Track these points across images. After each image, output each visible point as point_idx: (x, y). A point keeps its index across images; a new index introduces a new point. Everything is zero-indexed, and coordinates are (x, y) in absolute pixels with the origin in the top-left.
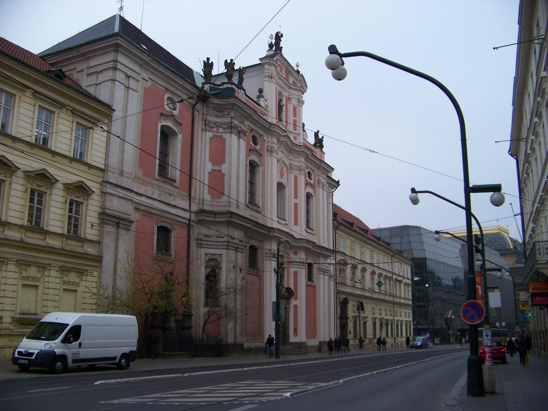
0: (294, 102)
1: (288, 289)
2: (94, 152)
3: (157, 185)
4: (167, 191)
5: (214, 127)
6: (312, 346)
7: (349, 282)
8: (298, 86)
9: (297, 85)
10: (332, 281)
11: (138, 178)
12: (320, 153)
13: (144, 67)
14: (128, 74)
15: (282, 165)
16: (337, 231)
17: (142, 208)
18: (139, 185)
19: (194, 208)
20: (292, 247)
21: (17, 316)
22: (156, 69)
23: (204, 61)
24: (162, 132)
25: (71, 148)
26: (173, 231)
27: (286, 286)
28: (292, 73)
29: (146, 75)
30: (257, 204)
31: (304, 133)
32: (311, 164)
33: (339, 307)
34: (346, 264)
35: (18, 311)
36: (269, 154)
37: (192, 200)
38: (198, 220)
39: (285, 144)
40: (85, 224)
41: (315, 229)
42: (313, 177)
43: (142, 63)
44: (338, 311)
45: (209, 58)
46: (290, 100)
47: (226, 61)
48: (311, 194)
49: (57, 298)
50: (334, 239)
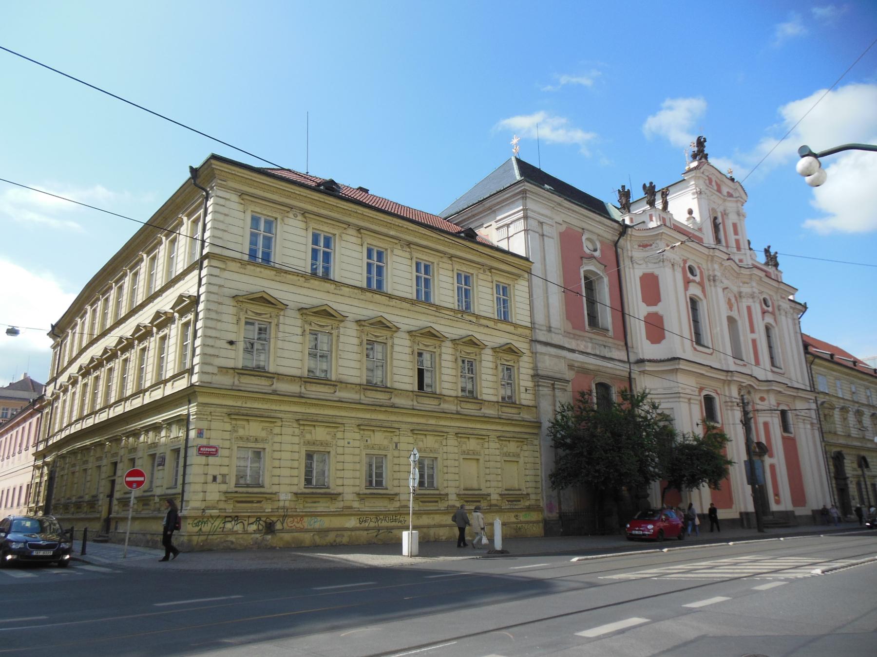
1: (759, 444)
2: (518, 311)
4: (601, 343)
6: (800, 516)
7: (840, 430)
10: (815, 431)
16: (812, 366)
18: (570, 340)
19: (633, 358)
21: (463, 492)
24: (586, 278)
25: (494, 310)
26: (613, 387)
27: (756, 441)
33: (831, 463)
34: (833, 408)
35: (462, 487)
36: (712, 283)
37: (629, 349)
40: (519, 389)
41: (783, 367)
42: (698, 272)
47: (644, 186)
49: (499, 471)
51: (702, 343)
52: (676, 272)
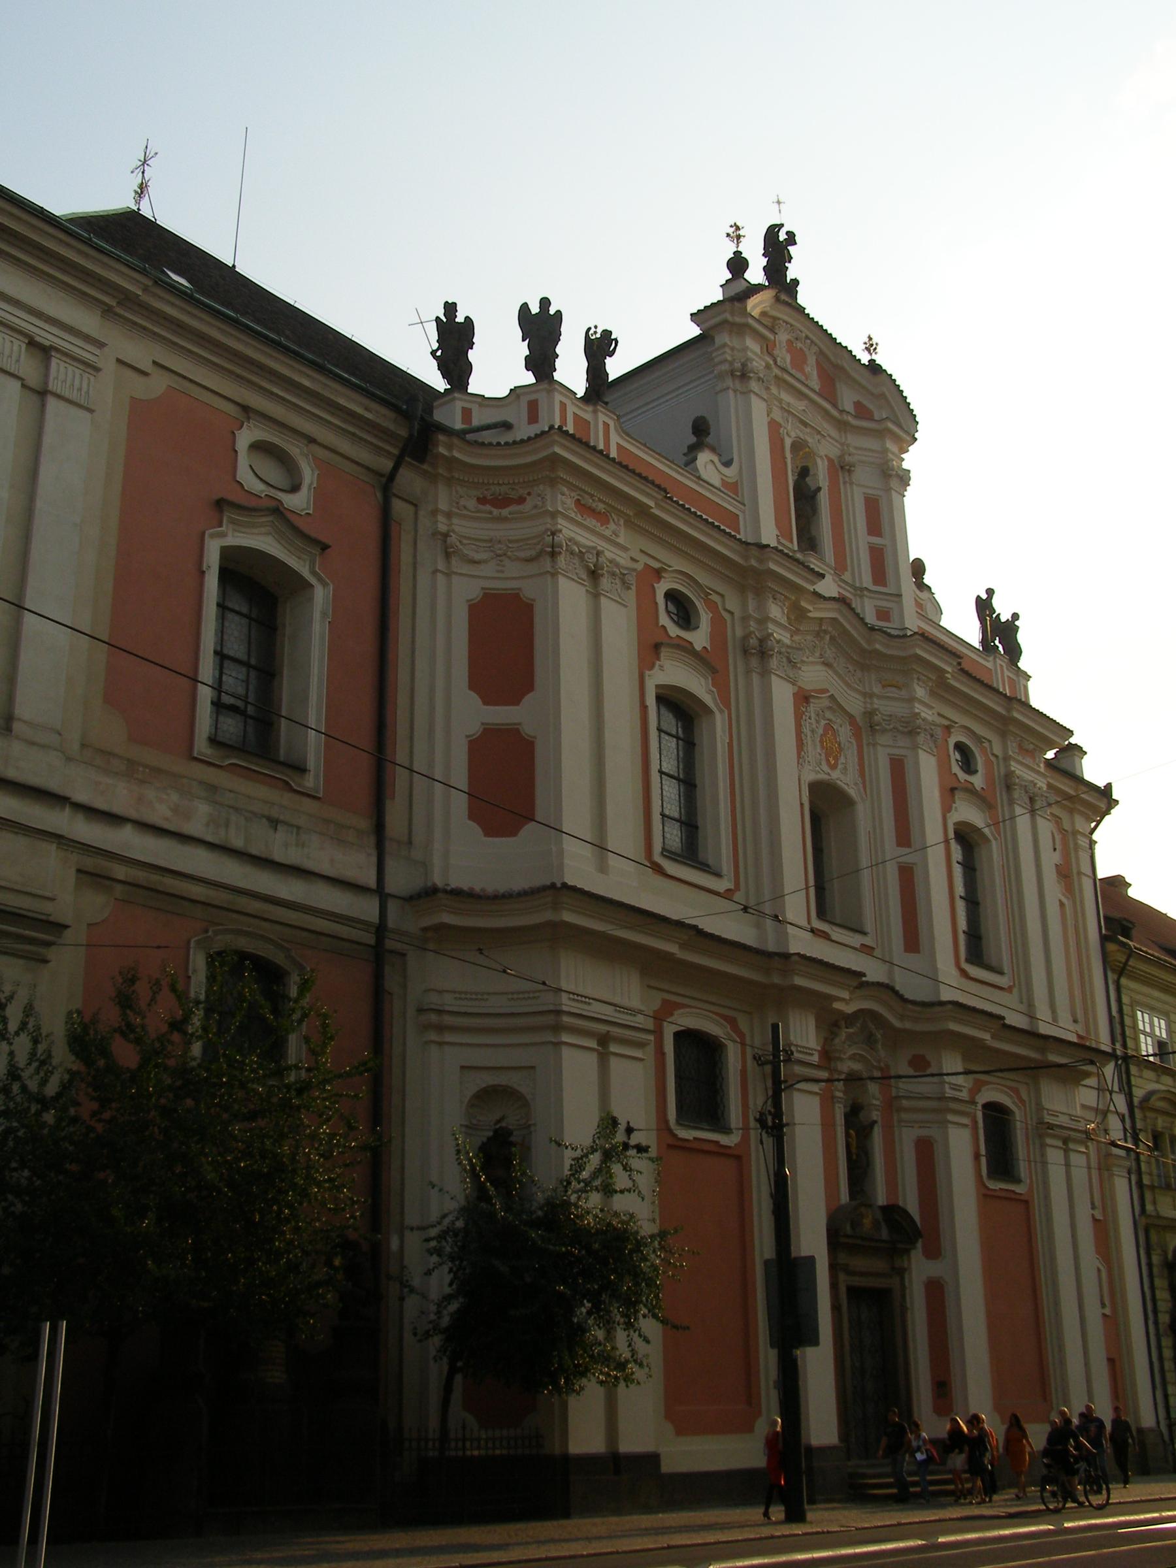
0: (865, 480)
1: (893, 1214)
3: (200, 782)
5: (485, 561)
8: (876, 418)
9: (873, 416)
11: (102, 752)
12: (1007, 673)
13: (120, 316)
14: (38, 339)
15: (828, 715)
16: (1123, 981)
17: (120, 872)
19: (399, 880)
20: (897, 1038)
22: (179, 327)
23: (438, 319)
27: (881, 1199)
28: (849, 376)
29: (140, 352)
30: (710, 862)
31: (924, 595)
32: (966, 712)
36: (754, 662)
37: (389, 847)
38: (425, 929)
39: (834, 633)
43: (112, 302)
44: (1159, 1303)
45: (454, 304)
46: (849, 471)
47: (524, 308)
48: (978, 830)
50: (1114, 1013)
51: (701, 856)
52: (603, 600)
